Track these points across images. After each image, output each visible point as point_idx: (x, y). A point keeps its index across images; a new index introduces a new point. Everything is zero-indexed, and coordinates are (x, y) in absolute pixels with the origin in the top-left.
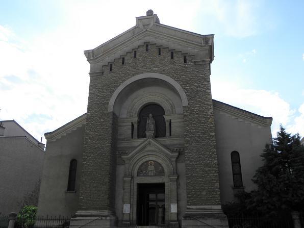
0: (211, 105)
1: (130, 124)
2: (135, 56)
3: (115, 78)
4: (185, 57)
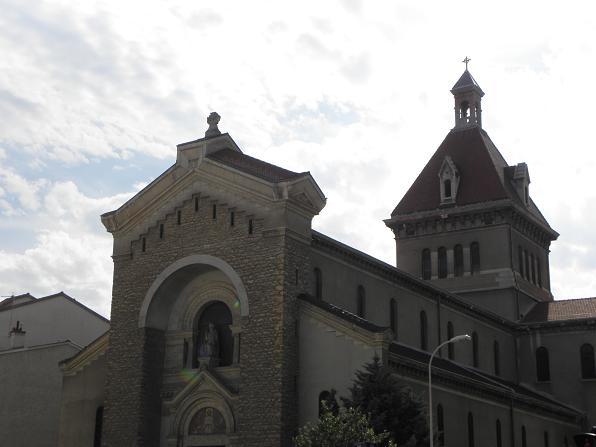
0: (280, 314)
1: (182, 342)
2: (179, 223)
3: (148, 265)
4: (251, 221)
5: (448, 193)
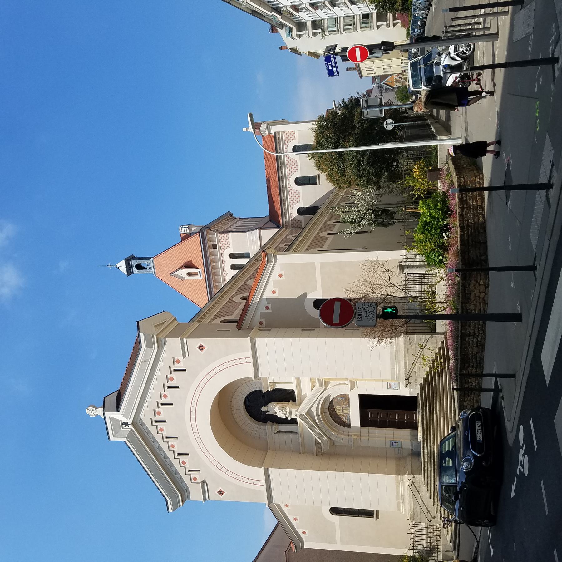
1: (277, 435)
5: (196, 274)
